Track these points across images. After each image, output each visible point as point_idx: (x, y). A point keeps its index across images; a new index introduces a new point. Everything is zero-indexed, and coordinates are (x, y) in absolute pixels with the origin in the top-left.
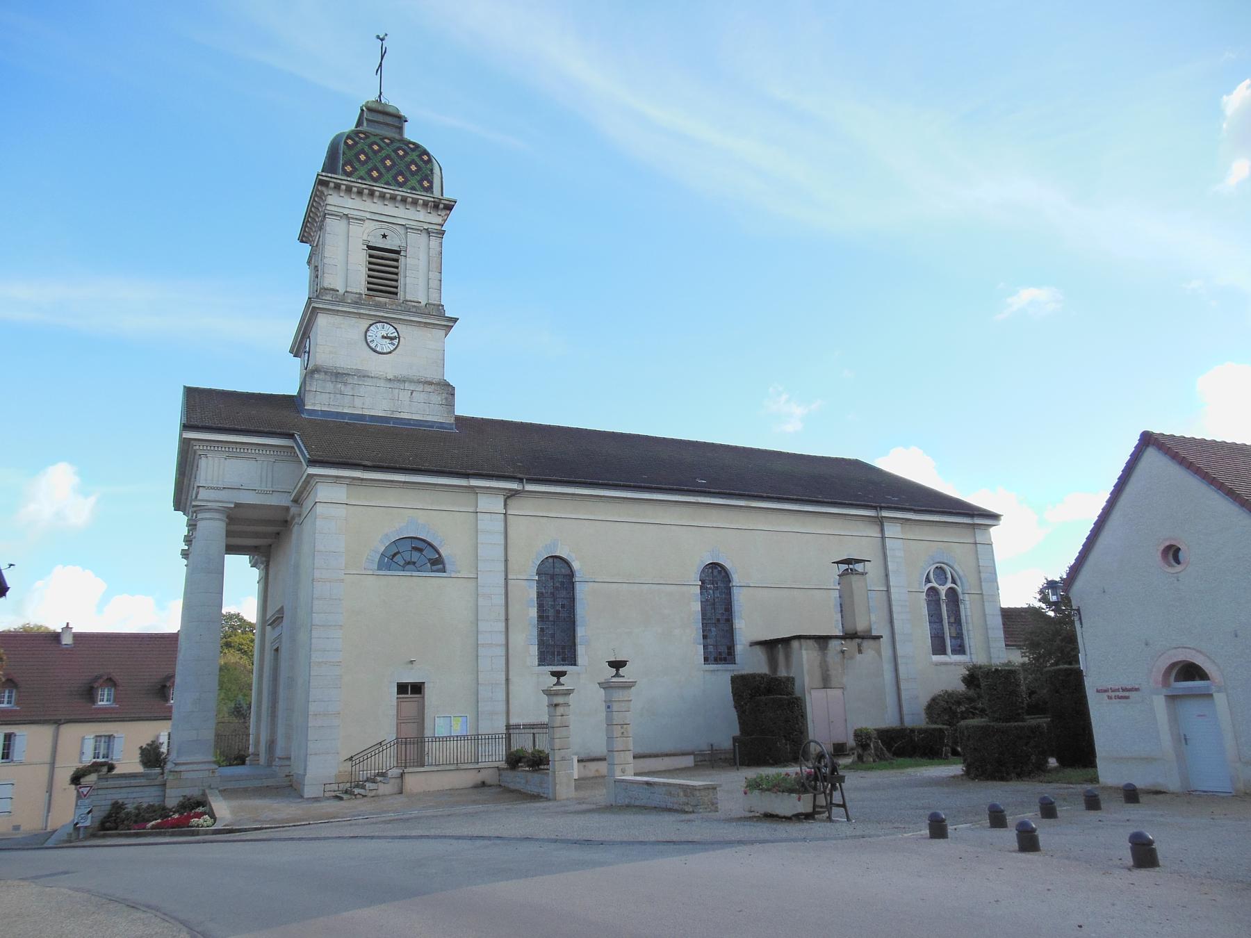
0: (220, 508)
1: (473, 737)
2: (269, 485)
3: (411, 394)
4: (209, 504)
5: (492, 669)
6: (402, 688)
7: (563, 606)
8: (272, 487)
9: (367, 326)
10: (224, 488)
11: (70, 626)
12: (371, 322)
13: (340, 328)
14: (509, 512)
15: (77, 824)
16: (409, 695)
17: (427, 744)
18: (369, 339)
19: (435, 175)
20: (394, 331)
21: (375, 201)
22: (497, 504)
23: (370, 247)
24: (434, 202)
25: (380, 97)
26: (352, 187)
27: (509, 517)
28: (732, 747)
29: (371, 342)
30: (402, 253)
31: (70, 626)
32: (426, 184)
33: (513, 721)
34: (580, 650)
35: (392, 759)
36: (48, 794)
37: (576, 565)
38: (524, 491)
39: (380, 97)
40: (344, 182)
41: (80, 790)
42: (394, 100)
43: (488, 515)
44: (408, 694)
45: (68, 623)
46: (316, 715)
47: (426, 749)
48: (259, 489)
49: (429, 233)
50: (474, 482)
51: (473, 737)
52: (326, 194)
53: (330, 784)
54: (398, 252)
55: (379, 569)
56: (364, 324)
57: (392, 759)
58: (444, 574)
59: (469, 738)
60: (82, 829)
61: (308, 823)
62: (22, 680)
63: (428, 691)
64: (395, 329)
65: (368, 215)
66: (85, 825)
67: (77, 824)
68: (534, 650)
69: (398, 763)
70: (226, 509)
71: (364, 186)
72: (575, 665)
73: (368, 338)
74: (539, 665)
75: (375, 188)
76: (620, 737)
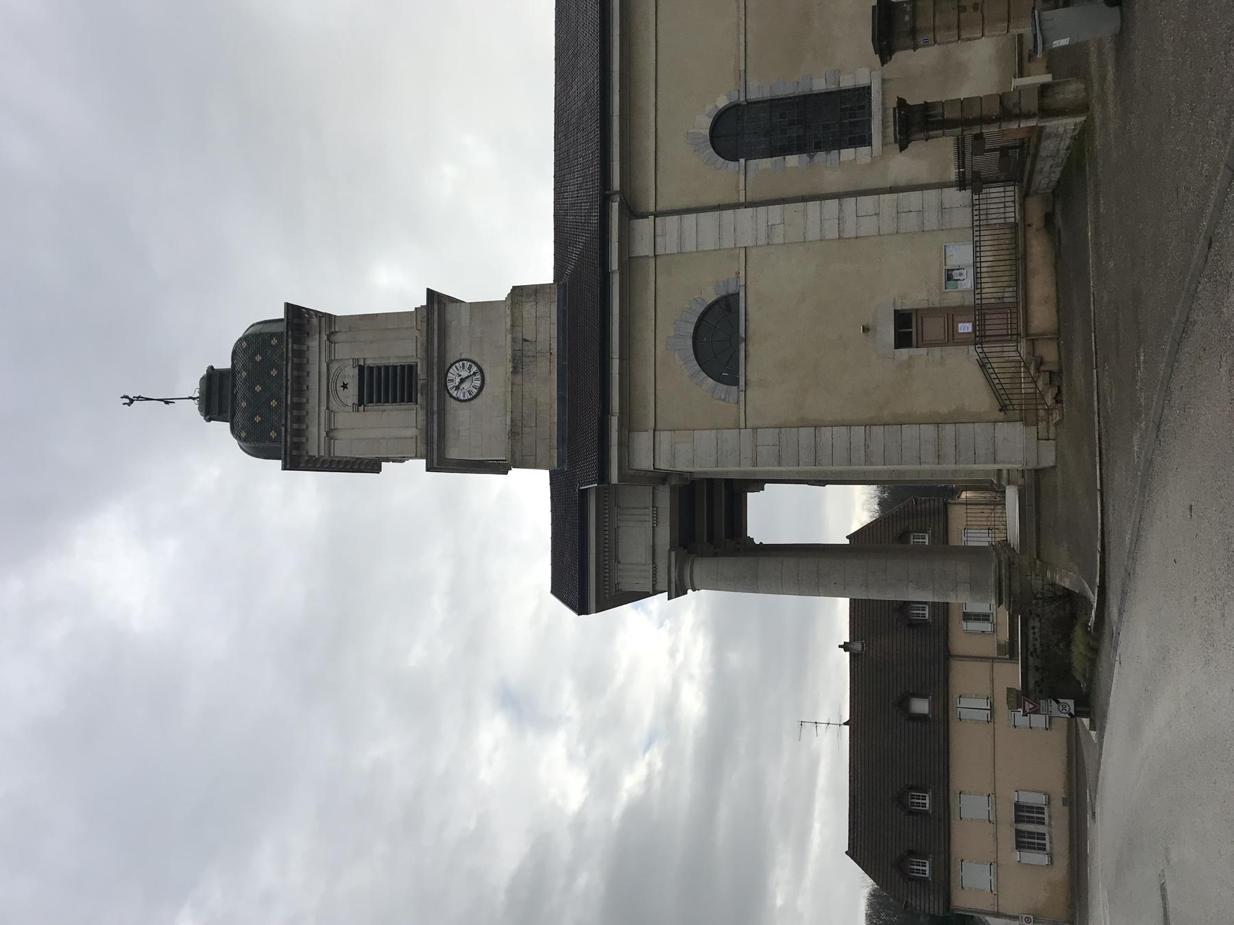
0: (677, 567)
1: (976, 213)
2: (646, 511)
3: (527, 341)
4: (673, 580)
5: (875, 214)
6: (903, 340)
7: (783, 116)
8: (648, 508)
9: (452, 400)
10: (653, 563)
11: (843, 644)
12: (447, 395)
13: (459, 431)
14: (652, 209)
15: (1070, 714)
16: (914, 330)
17: (984, 301)
18: (468, 396)
19: (262, 331)
20: (454, 367)
21: (305, 400)
22: (644, 227)
23: (361, 402)
24: (292, 331)
25: (194, 399)
26: (292, 429)
27: (661, 207)
28: (635, 468)
29: (470, 394)
30: (361, 363)
31: (843, 644)
32: (274, 342)
33: (953, 175)
34: (847, 82)
35: (1005, 349)
36: (1028, 222)
37: (722, 102)
38: (622, 192)
39: (194, 399)
40: (289, 439)
41: (1028, 711)
42: (192, 386)
43: (658, 239)
44: (911, 332)
45: (840, 646)
46: (939, 455)
47: (993, 301)
48: (651, 523)
49: (332, 333)
50: (614, 265)
51: (976, 213)
52: (307, 458)
53: (1038, 433)
54: (361, 369)
55: (735, 382)
56: (452, 404)
57: (1005, 349)
58: (742, 294)
59: (978, 239)
60: (1078, 709)
61: (1098, 493)
62: (892, 795)
63: (908, 305)
64: (452, 365)
65: (324, 408)
66: (1072, 707)
67: (1070, 714)
68: (847, 154)
69: (1010, 341)
70: (677, 567)
71: (289, 416)
72: (869, 88)
73: (466, 398)
74: (870, 144)
75: (289, 402)
76: (982, 12)
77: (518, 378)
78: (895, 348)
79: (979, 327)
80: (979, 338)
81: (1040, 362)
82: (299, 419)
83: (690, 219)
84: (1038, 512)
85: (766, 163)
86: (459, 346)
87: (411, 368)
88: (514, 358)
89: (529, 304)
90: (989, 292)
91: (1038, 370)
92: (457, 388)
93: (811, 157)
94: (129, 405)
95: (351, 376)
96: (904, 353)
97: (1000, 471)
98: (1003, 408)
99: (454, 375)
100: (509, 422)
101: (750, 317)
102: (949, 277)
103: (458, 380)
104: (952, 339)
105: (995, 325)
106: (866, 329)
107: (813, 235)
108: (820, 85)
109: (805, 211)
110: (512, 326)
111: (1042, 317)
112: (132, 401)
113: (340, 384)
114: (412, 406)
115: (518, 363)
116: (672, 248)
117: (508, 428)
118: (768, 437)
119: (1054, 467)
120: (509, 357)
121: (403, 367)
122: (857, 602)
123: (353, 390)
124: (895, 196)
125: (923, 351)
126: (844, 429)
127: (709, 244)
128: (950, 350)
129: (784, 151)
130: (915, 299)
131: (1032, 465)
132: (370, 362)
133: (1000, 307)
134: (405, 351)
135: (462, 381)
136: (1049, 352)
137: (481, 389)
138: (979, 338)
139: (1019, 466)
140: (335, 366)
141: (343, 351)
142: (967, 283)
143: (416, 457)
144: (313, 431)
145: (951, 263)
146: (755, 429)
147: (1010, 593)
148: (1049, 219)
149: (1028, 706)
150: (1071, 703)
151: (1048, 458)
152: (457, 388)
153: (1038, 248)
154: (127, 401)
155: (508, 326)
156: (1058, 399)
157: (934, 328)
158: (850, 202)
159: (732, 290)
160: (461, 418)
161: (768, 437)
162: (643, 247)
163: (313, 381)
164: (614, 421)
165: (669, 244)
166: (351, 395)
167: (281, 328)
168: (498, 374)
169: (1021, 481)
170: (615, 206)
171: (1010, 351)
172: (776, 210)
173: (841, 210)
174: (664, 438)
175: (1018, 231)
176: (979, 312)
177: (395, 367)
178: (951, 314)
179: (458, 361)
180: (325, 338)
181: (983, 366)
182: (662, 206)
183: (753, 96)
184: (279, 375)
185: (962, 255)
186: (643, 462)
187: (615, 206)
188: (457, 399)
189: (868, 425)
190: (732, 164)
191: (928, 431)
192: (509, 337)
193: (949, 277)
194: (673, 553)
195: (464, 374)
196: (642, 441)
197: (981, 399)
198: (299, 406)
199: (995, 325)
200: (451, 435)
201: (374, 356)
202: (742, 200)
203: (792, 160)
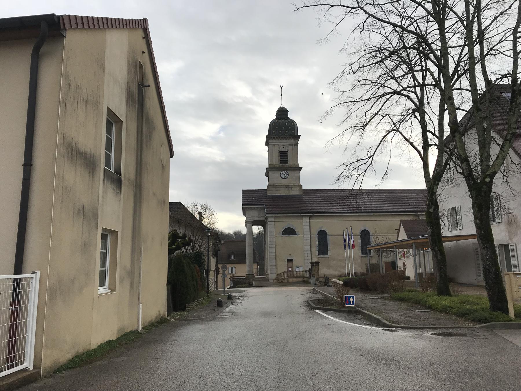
6: (288, 260)
14: (311, 220)
22: (308, 219)
23: (280, 151)
32: (293, 131)
34: (329, 252)
37: (327, 232)
50: (302, 215)
54: (287, 151)
68: (317, 252)
77: (284, 187)
78: (287, 259)
79: (290, 271)
80: (288, 271)
81: (284, 280)
82: (277, 138)
83: (309, 227)
84: (262, 280)
85: (317, 239)
86: (291, 173)
87: (287, 163)
88: (289, 186)
89: (299, 189)
90: (295, 273)
91: (283, 279)
92: (283, 173)
93: (317, 246)
94: (281, 87)
95: (285, 149)
96: (286, 261)
97: (268, 274)
98: (278, 275)
99: (285, 173)
100: (277, 184)
101: (293, 237)
102: (298, 267)
103: (284, 173)
104: (288, 268)
105: (290, 274)
106: (290, 255)
107: (305, 247)
108: (329, 247)
109: (309, 245)
110: (295, 185)
111: (291, 280)
112: (281, 88)
113: (284, 146)
114: (279, 163)
115: (288, 187)
116: (304, 224)
117: (275, 184)
118: (274, 240)
119: (269, 282)
120: (289, 184)
121: (287, 160)
122: (171, 206)
123: (283, 150)
124: (310, 259)
125: (287, 263)
126: (275, 252)
127: (305, 230)
128: (287, 267)
129: (319, 242)
130: (294, 262)
131: (269, 279)
132: (288, 153)
133: (293, 274)
134: (290, 162)
135: (284, 174)
136: (286, 281)
137: (283, 178)
138: (288, 271)
139: (269, 277)
140: (287, 145)
141: (291, 147)
142: (297, 270)
143: (269, 164)
144: (275, 141)
145: (300, 267)
146: (275, 238)
147: (249, 276)
148: (304, 281)
149: (231, 279)
150: (232, 285)
151: (270, 281)
152: (283, 173)
153: (301, 279)
154: (281, 87)
155: (295, 184)
156: (279, 282)
157: (290, 265)
158: (310, 252)
159: (297, 234)
160: (277, 174)
161: (274, 240)
162: (304, 219)
163: (284, 141)
164: (276, 215)
165: (305, 223)
166: (282, 149)
167: (296, 135)
168: (285, 182)
169: (267, 278)
170: (311, 215)
171: (286, 276)
172: (309, 241)
173: (309, 251)
174: (274, 223)
175: (304, 277)
176: (292, 271)
177: (287, 159)
178: (292, 267)
179: (288, 176)
180: (294, 143)
181: (284, 272)
182: (311, 222)
183: (328, 237)
184: (287, 123)
185: (301, 269)
186: (269, 220)
187: (311, 215)
188: (281, 173)
189: (276, 255)
190: (317, 234)
191: (274, 264)
192: (293, 184)
193: (298, 267)
194: (253, 221)
195: (285, 175)
196: (273, 219)
197: (279, 272)
198: (280, 138)
199: (290, 274)
200: (273, 172)
201: (289, 154)
202: (311, 235)
203: (317, 243)
